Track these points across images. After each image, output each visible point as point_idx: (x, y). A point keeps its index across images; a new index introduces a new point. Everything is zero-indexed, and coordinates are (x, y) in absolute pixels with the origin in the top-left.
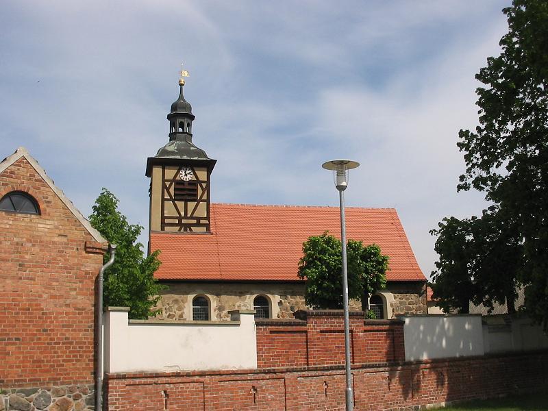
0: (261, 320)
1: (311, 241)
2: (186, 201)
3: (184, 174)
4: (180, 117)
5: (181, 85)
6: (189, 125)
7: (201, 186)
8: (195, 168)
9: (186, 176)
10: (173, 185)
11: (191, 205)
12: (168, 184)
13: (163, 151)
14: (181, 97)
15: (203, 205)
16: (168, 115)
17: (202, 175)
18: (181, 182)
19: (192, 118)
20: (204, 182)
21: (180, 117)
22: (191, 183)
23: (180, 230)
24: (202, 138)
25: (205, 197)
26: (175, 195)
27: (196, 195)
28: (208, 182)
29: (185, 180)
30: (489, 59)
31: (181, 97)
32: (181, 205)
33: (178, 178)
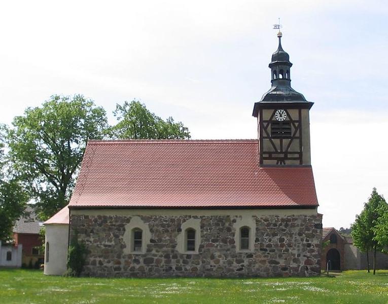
0: (308, 213)
1: (134, 102)
2: (281, 138)
3: (279, 115)
4: (281, 64)
5: (280, 37)
6: (288, 72)
7: (294, 125)
8: (288, 110)
9: (280, 116)
10: (270, 125)
11: (286, 142)
12: (265, 124)
13: (268, 97)
14: (280, 47)
15: (296, 142)
16: (270, 64)
17: (294, 114)
18: (277, 122)
19: (291, 65)
20: (297, 121)
21: (281, 64)
22: (284, 122)
23: (278, 163)
24: (299, 82)
25: (297, 135)
26: (272, 133)
27: (290, 133)
28: (300, 121)
29: (280, 120)
30: (292, 64)
31: (280, 47)
32: (277, 142)
33: (274, 119)
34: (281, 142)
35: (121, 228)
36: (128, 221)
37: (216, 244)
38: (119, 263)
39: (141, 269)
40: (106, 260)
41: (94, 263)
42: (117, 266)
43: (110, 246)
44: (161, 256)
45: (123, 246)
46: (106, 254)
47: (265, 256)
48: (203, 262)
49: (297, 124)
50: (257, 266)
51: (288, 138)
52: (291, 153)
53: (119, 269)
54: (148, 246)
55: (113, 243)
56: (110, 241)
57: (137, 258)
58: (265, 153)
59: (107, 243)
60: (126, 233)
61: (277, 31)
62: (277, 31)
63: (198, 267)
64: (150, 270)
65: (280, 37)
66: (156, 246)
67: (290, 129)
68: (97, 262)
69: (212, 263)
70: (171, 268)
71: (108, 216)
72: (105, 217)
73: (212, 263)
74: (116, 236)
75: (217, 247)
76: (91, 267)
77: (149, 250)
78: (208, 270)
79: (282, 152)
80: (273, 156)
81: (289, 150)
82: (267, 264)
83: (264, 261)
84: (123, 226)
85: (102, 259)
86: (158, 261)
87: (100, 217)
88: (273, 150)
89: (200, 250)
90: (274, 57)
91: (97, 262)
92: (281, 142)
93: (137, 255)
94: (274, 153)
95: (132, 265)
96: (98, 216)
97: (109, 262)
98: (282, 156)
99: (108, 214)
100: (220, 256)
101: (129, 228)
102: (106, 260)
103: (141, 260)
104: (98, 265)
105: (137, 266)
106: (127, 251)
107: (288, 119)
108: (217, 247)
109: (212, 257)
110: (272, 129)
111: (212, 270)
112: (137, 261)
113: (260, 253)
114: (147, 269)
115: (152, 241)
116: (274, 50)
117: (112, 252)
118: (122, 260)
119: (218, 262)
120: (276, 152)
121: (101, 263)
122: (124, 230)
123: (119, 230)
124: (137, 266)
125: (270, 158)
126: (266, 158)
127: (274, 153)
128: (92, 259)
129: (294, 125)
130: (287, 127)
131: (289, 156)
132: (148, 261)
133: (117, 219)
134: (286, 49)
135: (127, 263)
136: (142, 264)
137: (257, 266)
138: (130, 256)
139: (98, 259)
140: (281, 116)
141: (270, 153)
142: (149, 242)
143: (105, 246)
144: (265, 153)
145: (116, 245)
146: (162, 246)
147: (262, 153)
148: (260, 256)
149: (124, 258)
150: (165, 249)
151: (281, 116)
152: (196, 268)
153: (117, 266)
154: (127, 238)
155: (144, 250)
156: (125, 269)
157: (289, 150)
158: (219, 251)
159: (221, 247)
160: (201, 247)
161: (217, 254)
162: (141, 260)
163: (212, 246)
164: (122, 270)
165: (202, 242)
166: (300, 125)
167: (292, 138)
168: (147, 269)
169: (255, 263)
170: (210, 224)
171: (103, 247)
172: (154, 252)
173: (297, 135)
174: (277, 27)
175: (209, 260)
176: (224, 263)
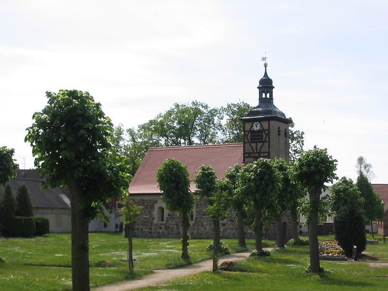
2: (257, 143)
5: (266, 67)
7: (265, 132)
8: (262, 123)
11: (259, 145)
12: (247, 133)
14: (266, 74)
15: (266, 144)
18: (254, 132)
20: (267, 130)
22: (259, 131)
25: (267, 140)
27: (262, 139)
28: (269, 130)
31: (266, 74)
32: (254, 145)
34: (257, 145)
35: (152, 207)
36: (156, 202)
37: (204, 217)
38: (151, 229)
39: (163, 232)
40: (144, 227)
41: (138, 229)
42: (150, 231)
43: (146, 218)
44: (174, 225)
45: (153, 219)
46: (144, 223)
47: (233, 225)
48: (197, 229)
49: (267, 132)
50: (228, 231)
51: (261, 142)
52: (262, 153)
53: (151, 233)
54: (167, 218)
55: (148, 216)
56: (146, 215)
57: (161, 226)
58: (247, 153)
59: (145, 217)
60: (155, 210)
61: (264, 62)
62: (264, 62)
63: (195, 232)
64: (168, 233)
65: (266, 67)
66: (171, 218)
67: (262, 136)
68: (140, 229)
69: (202, 229)
70: (179, 232)
71: (145, 199)
72: (144, 200)
73: (202, 229)
74: (150, 212)
75: (205, 219)
76: (136, 231)
77: (167, 221)
78: (200, 234)
79: (256, 153)
80: (252, 155)
81: (262, 151)
82: (234, 231)
83: (233, 228)
84: (153, 205)
85: (142, 227)
86: (173, 228)
87: (141, 200)
88: (251, 151)
89: (195, 221)
90: (261, 82)
91: (140, 229)
92: (257, 145)
93: (161, 224)
94: (252, 153)
95: (158, 230)
96: (285, 222)
97: (146, 228)
98: (257, 155)
99: (145, 198)
100: (207, 225)
101: (157, 206)
102: (144, 227)
103: (163, 227)
104: (140, 230)
105: (161, 231)
106: (155, 221)
107: (261, 129)
108: (205, 219)
109: (202, 226)
110: (251, 136)
111: (202, 234)
112: (161, 228)
113: (229, 223)
114: (166, 233)
115: (169, 215)
116: (261, 76)
117: (147, 222)
118: (153, 227)
119: (205, 228)
120: (253, 153)
121: (142, 229)
122: (154, 208)
123: (151, 208)
124: (161, 231)
125: (249, 157)
126: (247, 157)
127: (252, 153)
128: (137, 227)
129: (265, 132)
130: (260, 134)
131: (262, 155)
132: (167, 228)
133: (150, 201)
134: (270, 76)
135: (156, 229)
136: (163, 230)
137: (228, 231)
138: (157, 224)
139: (140, 227)
140: (257, 127)
141: (249, 153)
142: (167, 216)
143: (144, 218)
144: (247, 153)
145: (149, 218)
146: (175, 218)
147: (244, 153)
148: (230, 225)
149: (154, 226)
150: (176, 220)
151: (257, 127)
152: (169, 227)
153: (150, 231)
154: (156, 213)
155: (164, 222)
156: (155, 233)
157: (262, 151)
158: (206, 221)
159: (207, 219)
160: (196, 219)
161: (205, 223)
162: (163, 227)
163: (202, 218)
164: (153, 234)
165: (196, 215)
166: (269, 132)
167: (265, 141)
168: (166, 233)
169: (227, 229)
170: (201, 203)
171: (142, 219)
172: (170, 222)
173: (267, 140)
174: (264, 59)
175: (200, 227)
176: (209, 229)
